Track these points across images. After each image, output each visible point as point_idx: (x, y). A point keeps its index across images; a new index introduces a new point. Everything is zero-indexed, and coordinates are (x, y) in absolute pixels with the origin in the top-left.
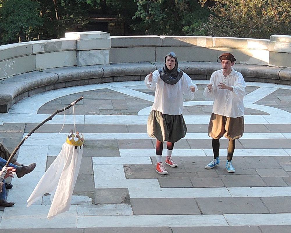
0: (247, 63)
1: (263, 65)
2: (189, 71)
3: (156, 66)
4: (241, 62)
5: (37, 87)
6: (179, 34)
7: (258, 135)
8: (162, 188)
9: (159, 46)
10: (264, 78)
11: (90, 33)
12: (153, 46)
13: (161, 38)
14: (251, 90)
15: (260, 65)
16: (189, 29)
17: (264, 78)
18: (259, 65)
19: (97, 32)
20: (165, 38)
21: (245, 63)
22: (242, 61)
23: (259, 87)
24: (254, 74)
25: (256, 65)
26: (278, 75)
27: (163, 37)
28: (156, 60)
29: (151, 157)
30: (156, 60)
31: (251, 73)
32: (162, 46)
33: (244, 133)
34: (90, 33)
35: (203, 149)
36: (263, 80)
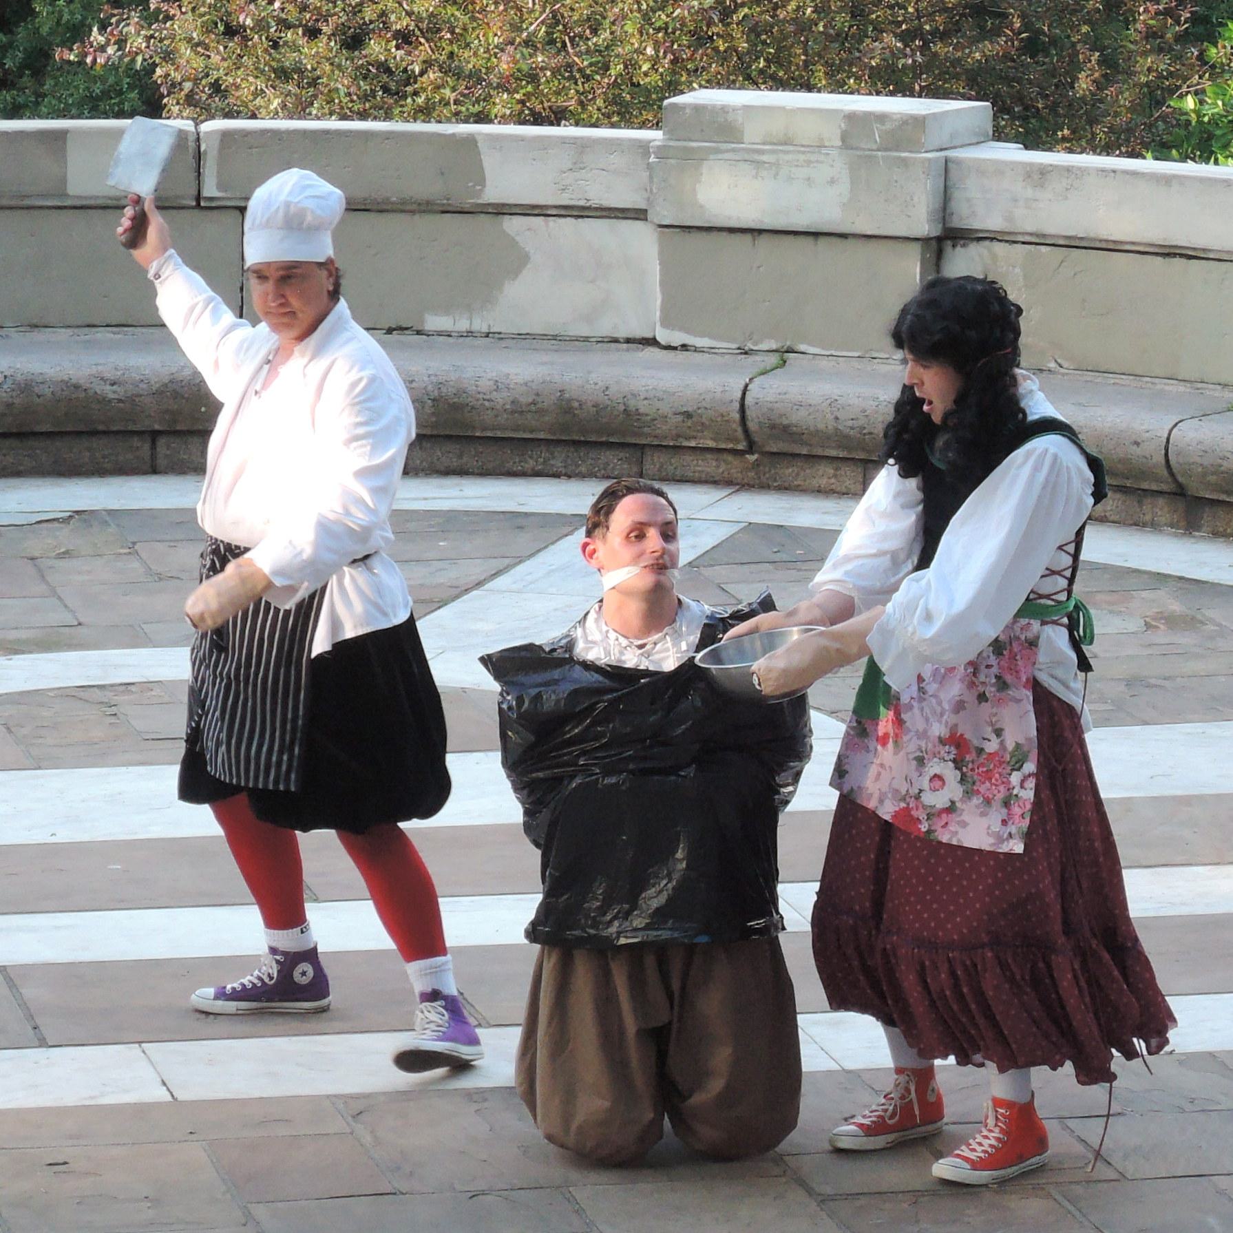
0: (479, 325)
21: (463, 325)
26: (737, 416)
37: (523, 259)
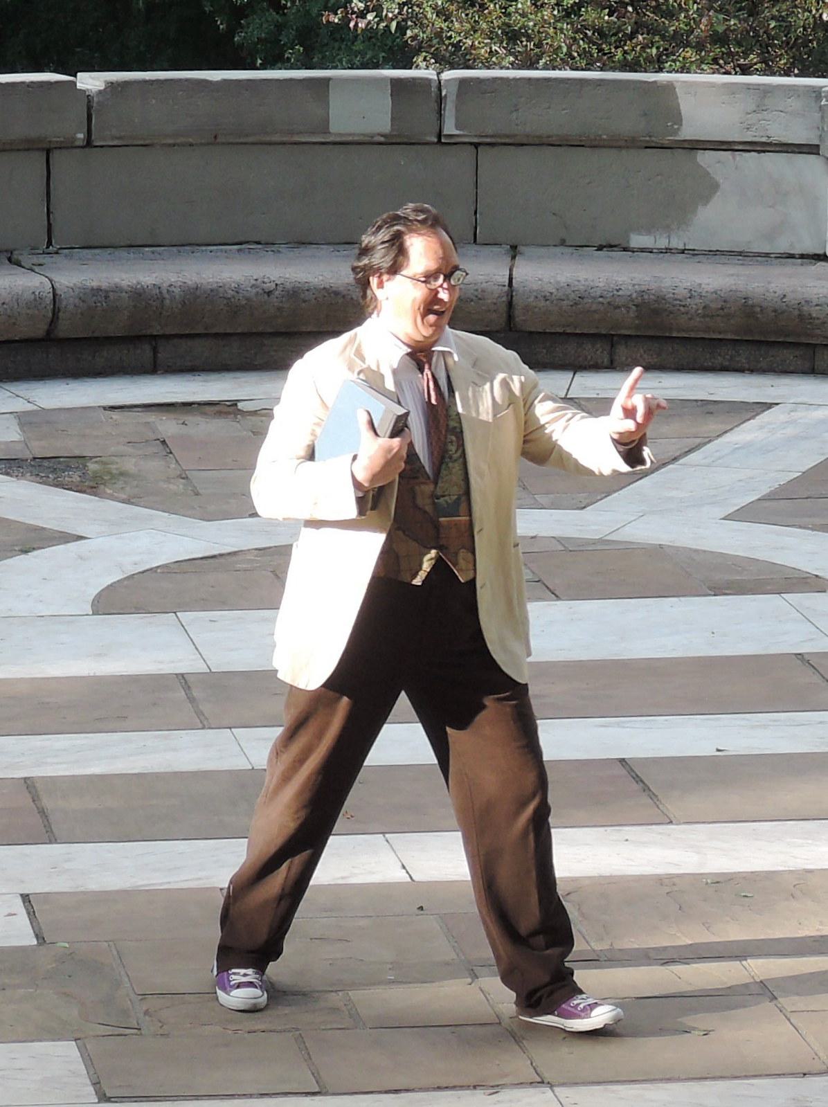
0: (677, 243)
1: (792, 256)
2: (279, 309)
3: (51, 281)
4: (637, 240)
5: (757, 261)
6: (87, 70)
7: (765, 726)
8: (108, 1100)
9: (68, 145)
10: (796, 345)
11: (32, 76)
12: (28, 146)
13: (79, 86)
14: (712, 426)
15: (767, 255)
16: (280, 27)
17: (796, 345)
18: (759, 255)
19: (260, 73)
20: (111, 85)
21: (662, 243)
22: (649, 229)
23: (769, 406)
24: (729, 316)
25: (740, 254)
27: (90, 82)
28: (50, 243)
29: (26, 898)
30: (50, 243)
31: (707, 313)
32: (89, 143)
33: (227, 886)
34: (310, 73)
35: (383, 833)
36: (788, 355)
37: (715, 187)
